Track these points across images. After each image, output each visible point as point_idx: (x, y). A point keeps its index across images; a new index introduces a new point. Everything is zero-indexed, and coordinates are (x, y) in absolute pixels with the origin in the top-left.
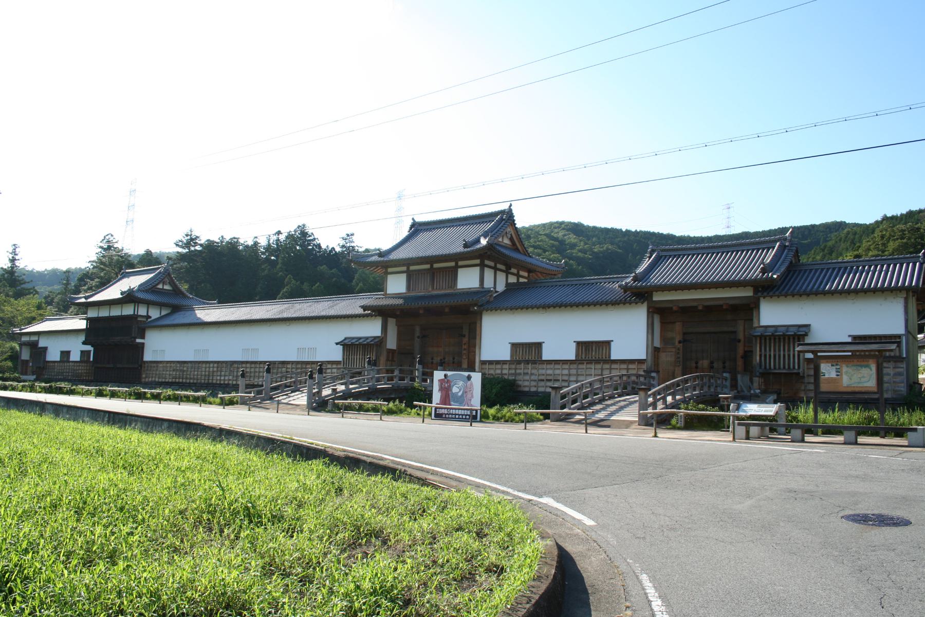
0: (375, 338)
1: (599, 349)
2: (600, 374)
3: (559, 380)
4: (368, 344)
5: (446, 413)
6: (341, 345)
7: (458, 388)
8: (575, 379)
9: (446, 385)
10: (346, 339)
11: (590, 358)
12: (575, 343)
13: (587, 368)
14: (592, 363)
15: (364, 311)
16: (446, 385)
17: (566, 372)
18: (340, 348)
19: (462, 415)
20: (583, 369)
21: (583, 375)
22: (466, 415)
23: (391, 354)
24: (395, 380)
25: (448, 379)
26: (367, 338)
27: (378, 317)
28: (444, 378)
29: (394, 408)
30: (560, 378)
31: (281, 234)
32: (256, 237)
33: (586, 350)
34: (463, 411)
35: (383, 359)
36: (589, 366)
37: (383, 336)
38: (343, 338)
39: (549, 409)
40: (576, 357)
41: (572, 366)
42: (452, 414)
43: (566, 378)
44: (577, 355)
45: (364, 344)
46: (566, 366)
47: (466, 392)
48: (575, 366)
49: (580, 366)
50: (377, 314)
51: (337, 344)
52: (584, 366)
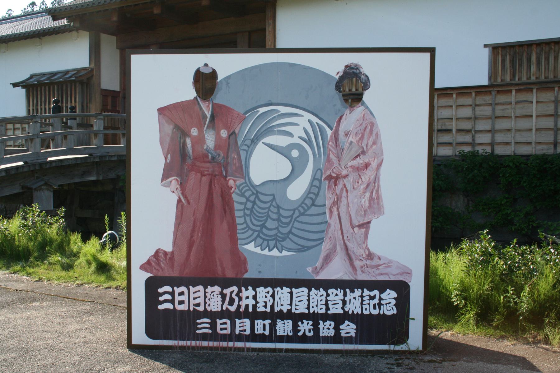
0: (79, 70)
1: (547, 59)
2: (552, 112)
3: (450, 131)
4: (66, 82)
5: (215, 305)
6: (23, 87)
7: (284, 152)
8: (488, 127)
9: (210, 140)
10: (32, 77)
11: (524, 79)
12: (487, 49)
13: (517, 103)
14: (531, 90)
15: (54, 19)
16: (210, 140)
17: (467, 112)
18: (21, 92)
19: (315, 318)
20: (510, 103)
21: (510, 117)
22: (338, 319)
23: (110, 99)
24: (95, 141)
25: (220, 98)
26: (66, 72)
27: (80, 31)
28: (190, 93)
29: (22, 240)
30: (454, 126)
31: (35, 5)
32: (10, 10)
33: (512, 62)
34: (318, 295)
35: (94, 108)
36: (523, 96)
37: (93, 65)
38: (28, 76)
39: (120, 145)
40: (490, 78)
41: (480, 100)
42: (254, 315)
43: (466, 125)
44: (492, 75)
45: (60, 82)
46: (468, 100)
47: (334, 179)
48: (488, 99)
49: (502, 98)
50: (78, 25)
51: (15, 85)
52: (513, 97)
